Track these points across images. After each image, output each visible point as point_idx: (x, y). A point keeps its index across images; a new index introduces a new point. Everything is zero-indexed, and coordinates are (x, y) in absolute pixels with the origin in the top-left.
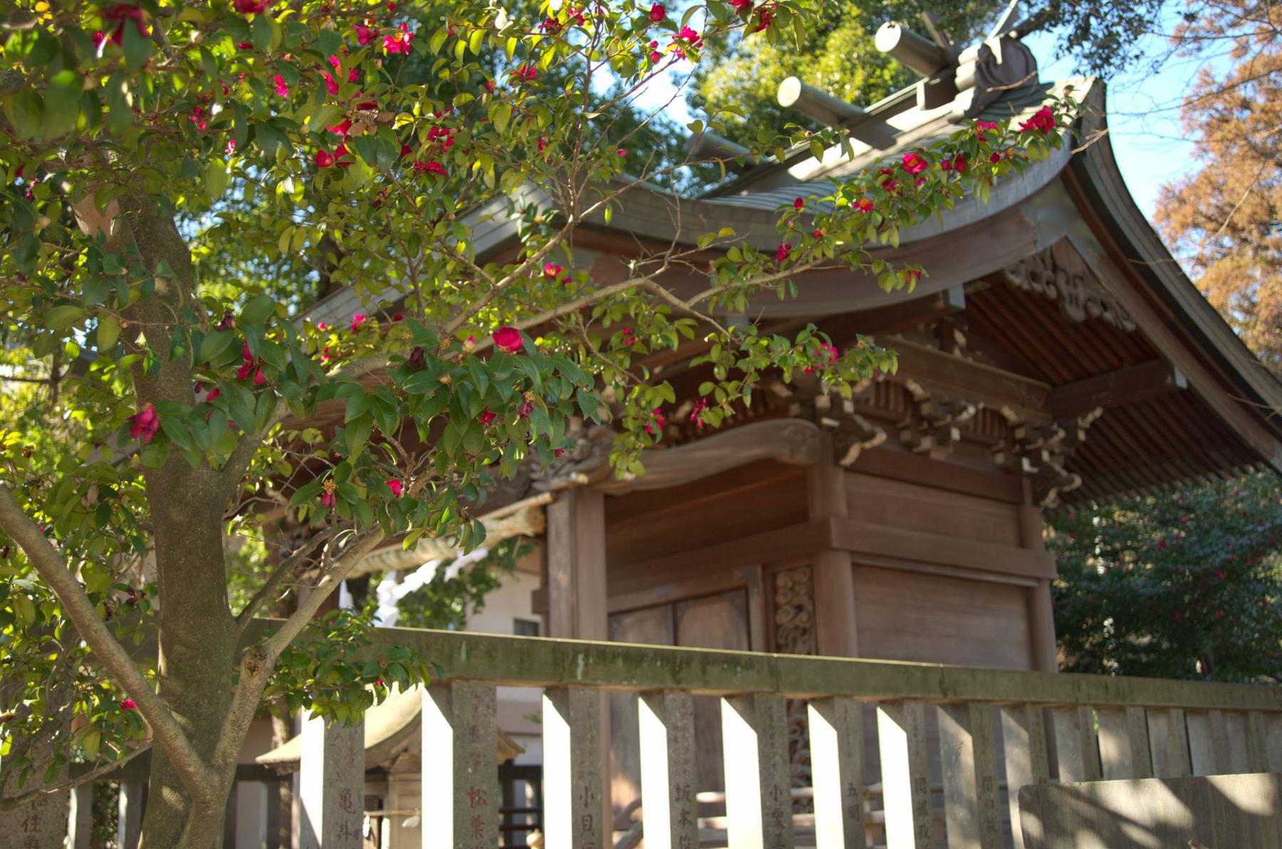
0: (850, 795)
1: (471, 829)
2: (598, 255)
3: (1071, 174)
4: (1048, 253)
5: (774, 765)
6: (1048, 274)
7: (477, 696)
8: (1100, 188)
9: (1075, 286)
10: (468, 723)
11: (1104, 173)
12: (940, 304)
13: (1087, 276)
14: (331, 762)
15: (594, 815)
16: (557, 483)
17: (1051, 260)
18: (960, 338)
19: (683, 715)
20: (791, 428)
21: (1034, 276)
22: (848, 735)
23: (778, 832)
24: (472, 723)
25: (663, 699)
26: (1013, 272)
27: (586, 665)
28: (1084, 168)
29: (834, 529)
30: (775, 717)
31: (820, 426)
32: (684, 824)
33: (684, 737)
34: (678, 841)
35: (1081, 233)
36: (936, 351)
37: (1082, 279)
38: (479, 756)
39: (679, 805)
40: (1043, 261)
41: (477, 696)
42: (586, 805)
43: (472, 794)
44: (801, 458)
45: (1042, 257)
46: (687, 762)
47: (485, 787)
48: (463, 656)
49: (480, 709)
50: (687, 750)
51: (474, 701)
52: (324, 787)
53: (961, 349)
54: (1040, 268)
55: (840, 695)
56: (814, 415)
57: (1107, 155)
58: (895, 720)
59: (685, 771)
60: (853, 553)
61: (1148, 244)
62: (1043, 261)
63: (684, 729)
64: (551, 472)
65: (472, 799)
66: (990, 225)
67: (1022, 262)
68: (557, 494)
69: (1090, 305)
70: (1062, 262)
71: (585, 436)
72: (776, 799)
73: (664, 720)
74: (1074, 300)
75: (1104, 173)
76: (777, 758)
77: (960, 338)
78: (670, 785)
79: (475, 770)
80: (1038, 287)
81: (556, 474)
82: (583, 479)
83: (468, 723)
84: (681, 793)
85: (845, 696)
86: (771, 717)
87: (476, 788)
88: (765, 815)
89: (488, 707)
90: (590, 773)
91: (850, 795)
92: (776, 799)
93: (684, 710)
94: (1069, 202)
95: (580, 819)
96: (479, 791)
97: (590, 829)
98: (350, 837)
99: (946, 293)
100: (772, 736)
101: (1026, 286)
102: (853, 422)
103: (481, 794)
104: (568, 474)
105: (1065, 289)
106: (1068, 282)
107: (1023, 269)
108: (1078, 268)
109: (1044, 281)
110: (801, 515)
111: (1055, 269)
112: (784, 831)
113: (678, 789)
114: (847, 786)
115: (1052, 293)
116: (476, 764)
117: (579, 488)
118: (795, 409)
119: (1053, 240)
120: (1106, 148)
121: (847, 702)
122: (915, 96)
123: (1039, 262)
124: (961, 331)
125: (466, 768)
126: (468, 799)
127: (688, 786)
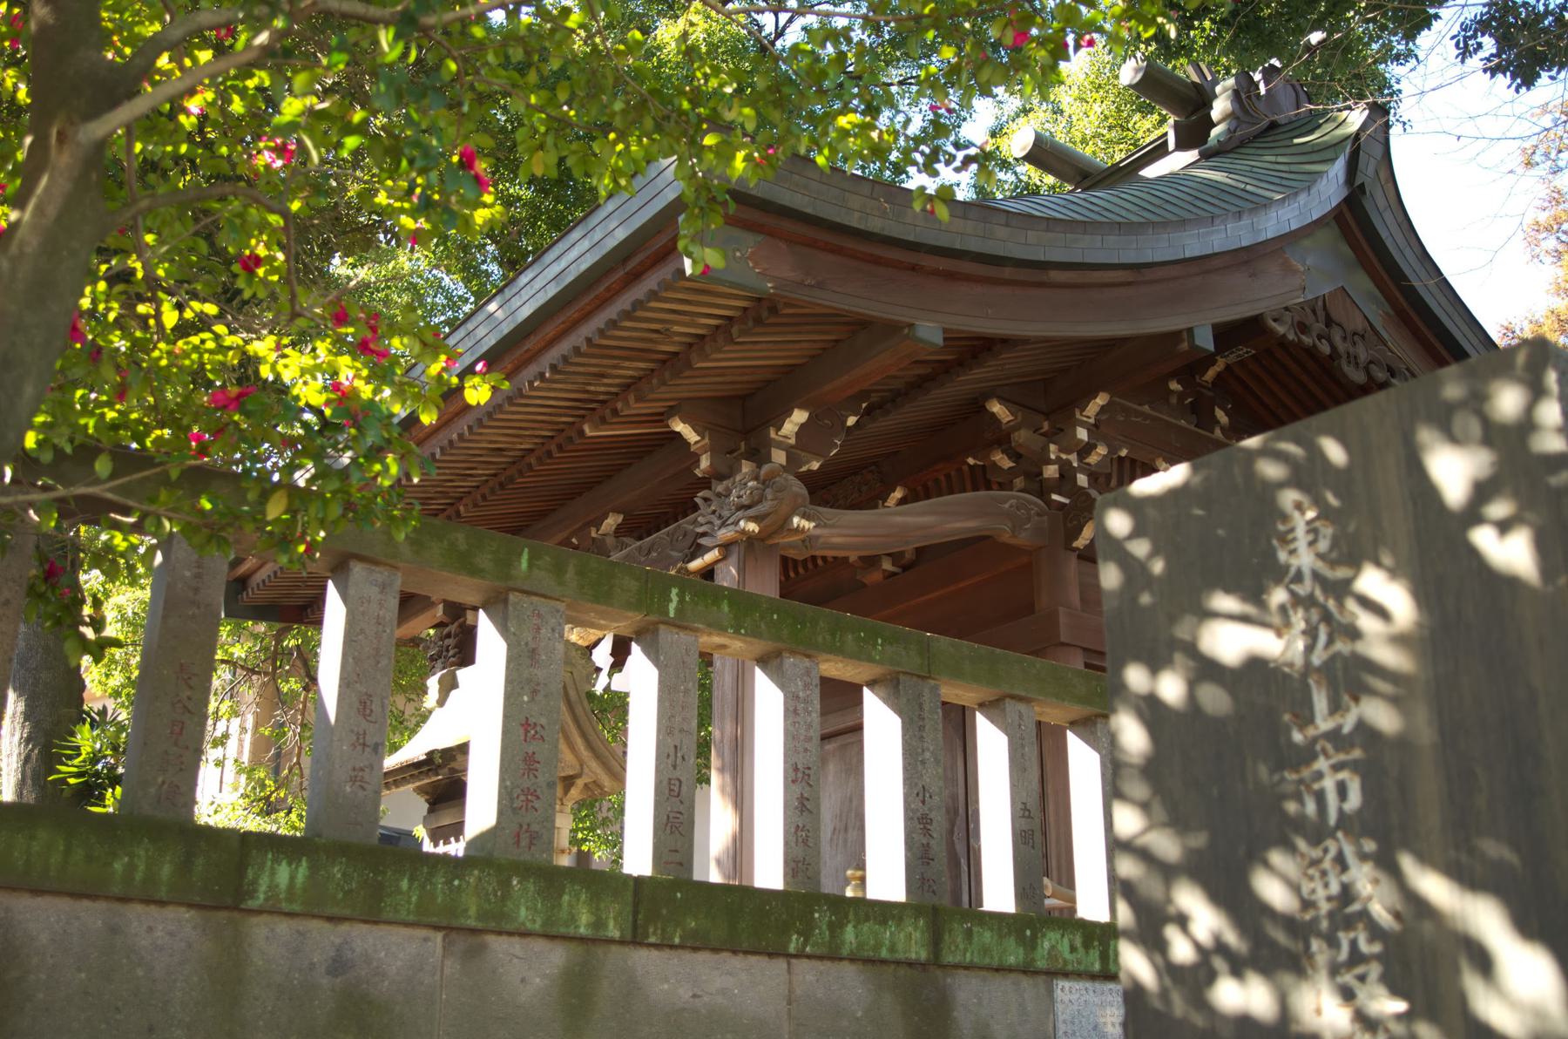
0: (1023, 816)
1: (522, 766)
2: (760, 238)
3: (1348, 216)
4: (1320, 303)
5: (923, 762)
6: (1319, 326)
7: (539, 615)
8: (1384, 234)
9: (1354, 343)
10: (527, 644)
11: (1388, 216)
12: (1185, 346)
13: (1368, 334)
14: (351, 660)
15: (682, 779)
16: (725, 534)
17: (1324, 313)
18: (1221, 415)
19: (806, 686)
20: (1013, 501)
21: (1303, 328)
22: (1023, 746)
23: (925, 842)
24: (532, 645)
25: (781, 664)
26: (1275, 320)
27: (681, 601)
28: (1363, 207)
29: (1063, 619)
30: (926, 707)
31: (1049, 503)
32: (802, 811)
33: (806, 710)
34: (793, 830)
35: (1361, 285)
36: (1192, 427)
37: (1363, 336)
38: (538, 684)
39: (797, 789)
40: (1314, 312)
41: (539, 615)
42: (675, 767)
43: (527, 725)
44: (1023, 539)
45: (1312, 306)
46: (809, 739)
47: (543, 721)
48: (524, 564)
49: (543, 631)
50: (810, 726)
51: (536, 621)
52: (340, 686)
53: (1222, 429)
54: (1310, 319)
55: (1012, 697)
56: (1042, 489)
57: (1413, 240)
58: (1087, 742)
59: (806, 750)
60: (1085, 649)
61: (1443, 301)
62: (1314, 312)
63: (806, 701)
64: (718, 522)
65: (527, 732)
66: (1247, 258)
67: (1287, 309)
68: (726, 547)
69: (1372, 366)
70: (1337, 314)
71: (756, 478)
72: (923, 802)
73: (782, 687)
74: (1353, 359)
75: (1388, 216)
76: (927, 755)
77: (1221, 415)
78: (785, 762)
79: (532, 700)
80: (1307, 340)
81: (723, 525)
82: (752, 527)
83: (527, 644)
84: (800, 775)
85: (1020, 699)
86: (921, 708)
87: (532, 721)
88: (909, 818)
89: (553, 630)
90: (681, 731)
91: (1023, 816)
92: (923, 802)
93: (809, 680)
94: (1345, 249)
95: (665, 783)
96: (535, 724)
97: (678, 795)
98: (367, 749)
99: (1190, 330)
100: (922, 728)
101: (1291, 337)
102: (1088, 495)
103: (538, 728)
104: (736, 523)
105: (1341, 347)
106: (1345, 339)
107: (1287, 317)
108: (1359, 324)
109: (1314, 334)
110: (1030, 608)
111: (1329, 322)
112: (932, 842)
113: (796, 770)
114: (1020, 806)
115: (1325, 348)
116: (534, 692)
117: (750, 541)
118: (1019, 482)
119: (1326, 290)
120: (1390, 185)
121: (1022, 707)
122: (1166, 142)
123: (1308, 310)
124: (1223, 409)
125: (520, 695)
126: (522, 731)
127: (809, 768)
